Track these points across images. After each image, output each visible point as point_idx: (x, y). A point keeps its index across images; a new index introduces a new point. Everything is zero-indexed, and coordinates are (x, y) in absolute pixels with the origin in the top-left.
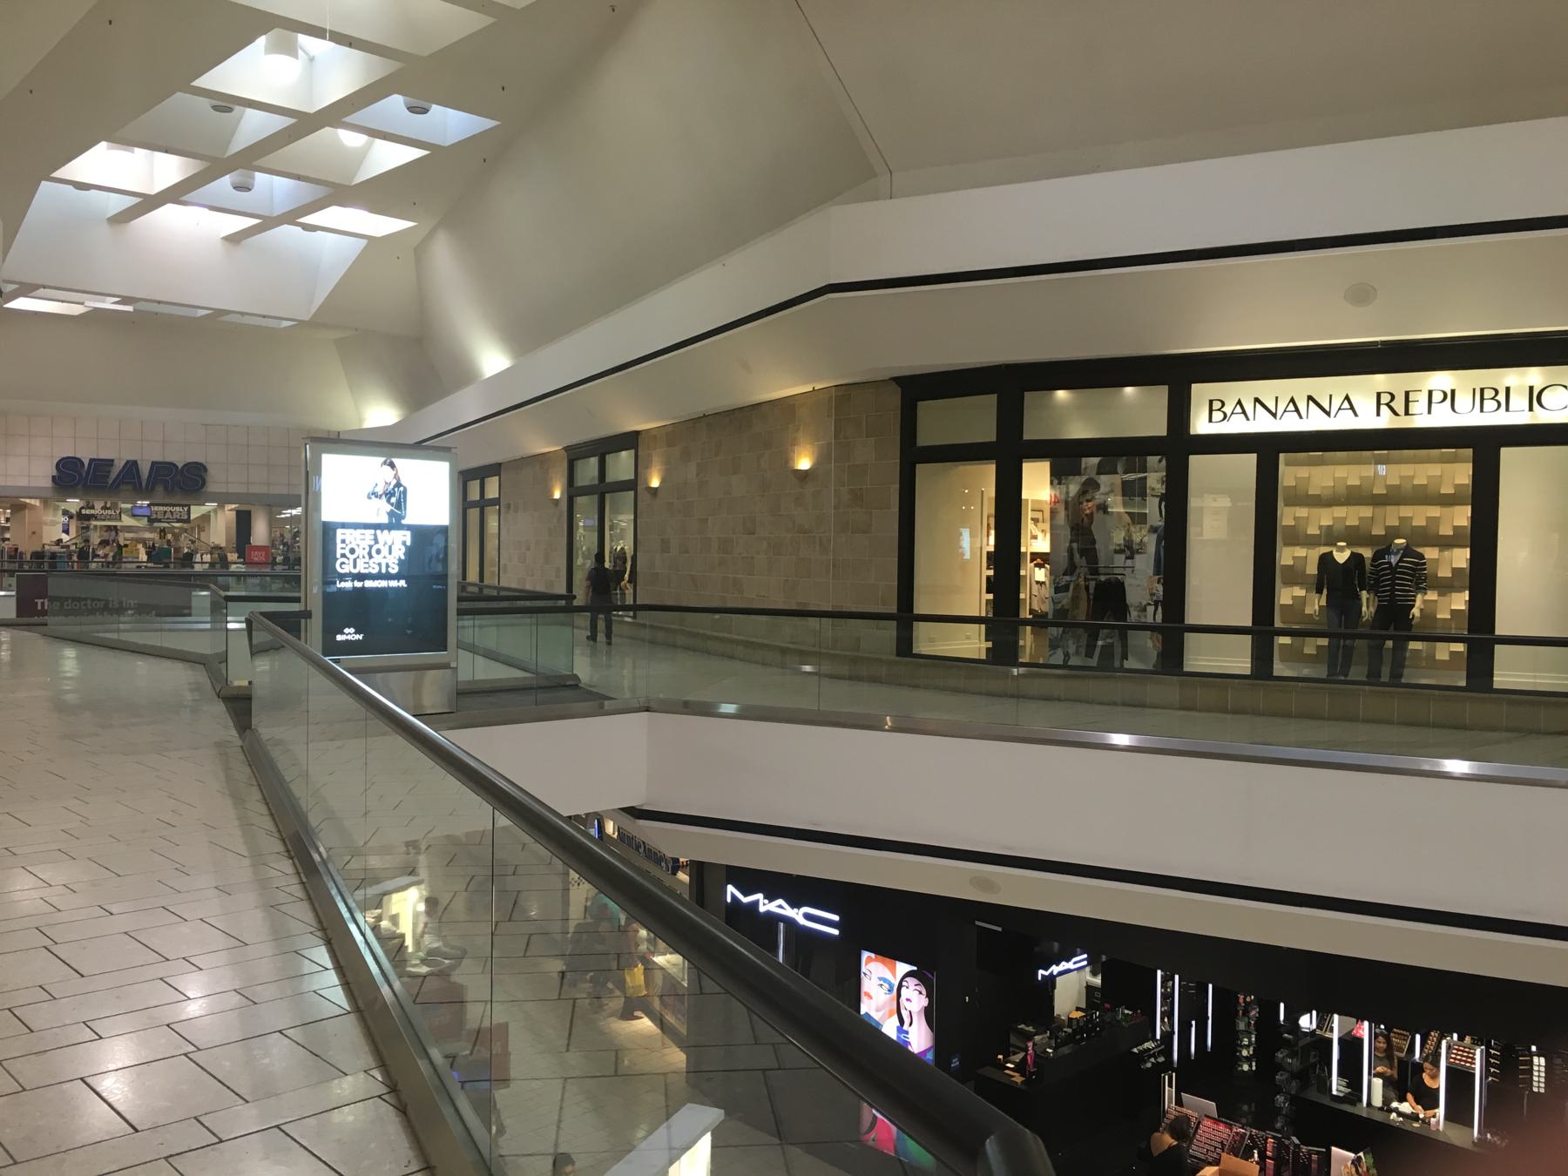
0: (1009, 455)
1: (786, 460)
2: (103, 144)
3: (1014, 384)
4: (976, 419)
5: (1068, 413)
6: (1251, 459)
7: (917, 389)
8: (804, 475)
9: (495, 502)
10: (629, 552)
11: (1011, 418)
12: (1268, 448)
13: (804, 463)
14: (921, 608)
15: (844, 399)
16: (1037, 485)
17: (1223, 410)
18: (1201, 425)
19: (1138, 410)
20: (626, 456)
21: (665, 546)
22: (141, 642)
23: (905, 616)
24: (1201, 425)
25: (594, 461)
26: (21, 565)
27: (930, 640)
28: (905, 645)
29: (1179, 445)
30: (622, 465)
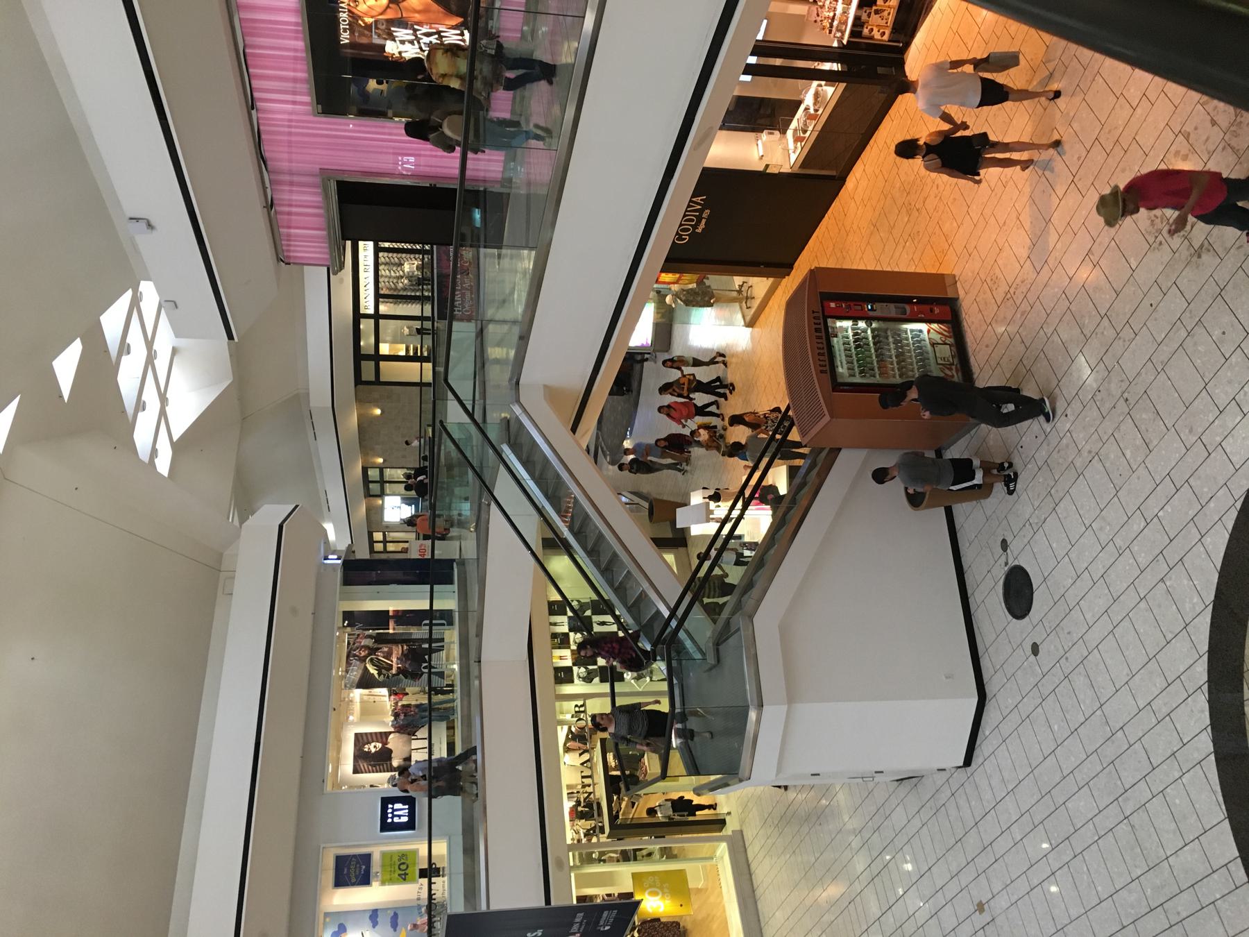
0: (377, 358)
1: (377, 417)
2: (102, 318)
3: (359, 357)
4: (367, 367)
5: (367, 342)
6: (381, 254)
7: (358, 380)
8: (383, 412)
9: (384, 536)
10: (405, 471)
11: (368, 357)
12: (378, 297)
13: (378, 412)
14: (417, 380)
15: (359, 400)
16: (385, 349)
17: (367, 305)
18: (371, 311)
19: (367, 326)
20: (370, 472)
21: (404, 457)
22: (524, 295)
23: (421, 385)
24: (371, 311)
25: (371, 486)
26: (447, 616)
27: (428, 377)
28: (428, 385)
29: (377, 316)
30: (373, 474)
